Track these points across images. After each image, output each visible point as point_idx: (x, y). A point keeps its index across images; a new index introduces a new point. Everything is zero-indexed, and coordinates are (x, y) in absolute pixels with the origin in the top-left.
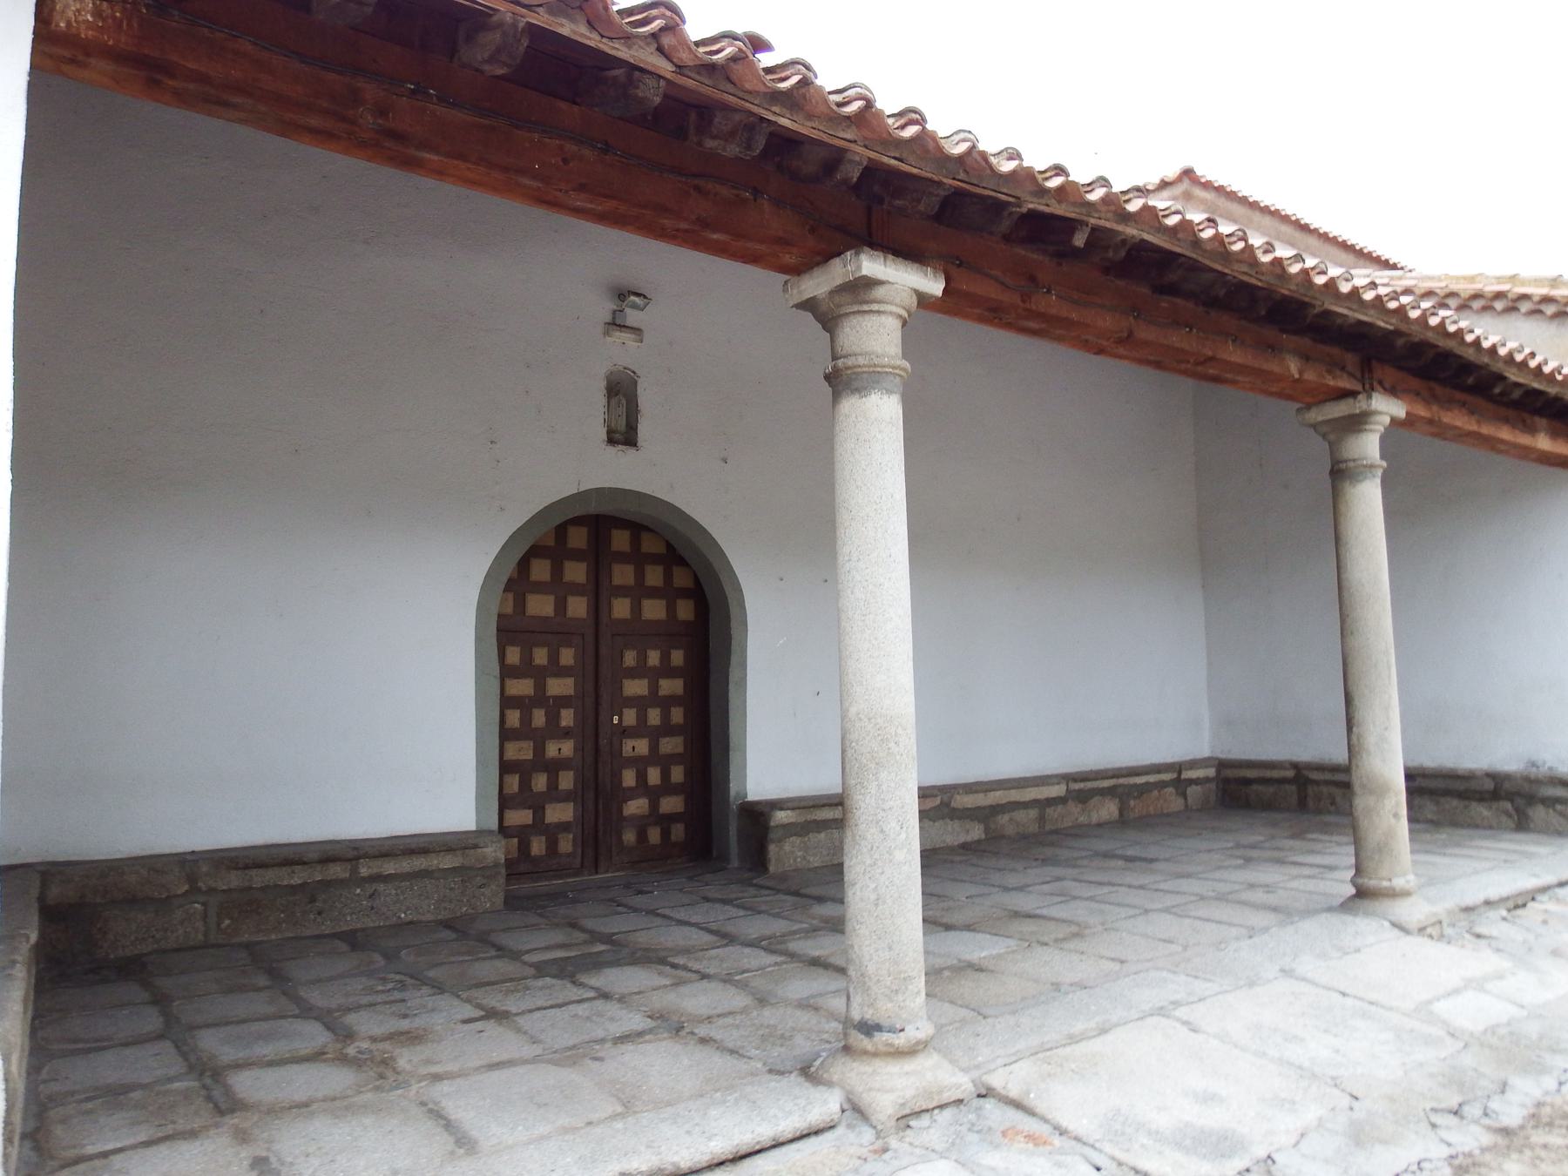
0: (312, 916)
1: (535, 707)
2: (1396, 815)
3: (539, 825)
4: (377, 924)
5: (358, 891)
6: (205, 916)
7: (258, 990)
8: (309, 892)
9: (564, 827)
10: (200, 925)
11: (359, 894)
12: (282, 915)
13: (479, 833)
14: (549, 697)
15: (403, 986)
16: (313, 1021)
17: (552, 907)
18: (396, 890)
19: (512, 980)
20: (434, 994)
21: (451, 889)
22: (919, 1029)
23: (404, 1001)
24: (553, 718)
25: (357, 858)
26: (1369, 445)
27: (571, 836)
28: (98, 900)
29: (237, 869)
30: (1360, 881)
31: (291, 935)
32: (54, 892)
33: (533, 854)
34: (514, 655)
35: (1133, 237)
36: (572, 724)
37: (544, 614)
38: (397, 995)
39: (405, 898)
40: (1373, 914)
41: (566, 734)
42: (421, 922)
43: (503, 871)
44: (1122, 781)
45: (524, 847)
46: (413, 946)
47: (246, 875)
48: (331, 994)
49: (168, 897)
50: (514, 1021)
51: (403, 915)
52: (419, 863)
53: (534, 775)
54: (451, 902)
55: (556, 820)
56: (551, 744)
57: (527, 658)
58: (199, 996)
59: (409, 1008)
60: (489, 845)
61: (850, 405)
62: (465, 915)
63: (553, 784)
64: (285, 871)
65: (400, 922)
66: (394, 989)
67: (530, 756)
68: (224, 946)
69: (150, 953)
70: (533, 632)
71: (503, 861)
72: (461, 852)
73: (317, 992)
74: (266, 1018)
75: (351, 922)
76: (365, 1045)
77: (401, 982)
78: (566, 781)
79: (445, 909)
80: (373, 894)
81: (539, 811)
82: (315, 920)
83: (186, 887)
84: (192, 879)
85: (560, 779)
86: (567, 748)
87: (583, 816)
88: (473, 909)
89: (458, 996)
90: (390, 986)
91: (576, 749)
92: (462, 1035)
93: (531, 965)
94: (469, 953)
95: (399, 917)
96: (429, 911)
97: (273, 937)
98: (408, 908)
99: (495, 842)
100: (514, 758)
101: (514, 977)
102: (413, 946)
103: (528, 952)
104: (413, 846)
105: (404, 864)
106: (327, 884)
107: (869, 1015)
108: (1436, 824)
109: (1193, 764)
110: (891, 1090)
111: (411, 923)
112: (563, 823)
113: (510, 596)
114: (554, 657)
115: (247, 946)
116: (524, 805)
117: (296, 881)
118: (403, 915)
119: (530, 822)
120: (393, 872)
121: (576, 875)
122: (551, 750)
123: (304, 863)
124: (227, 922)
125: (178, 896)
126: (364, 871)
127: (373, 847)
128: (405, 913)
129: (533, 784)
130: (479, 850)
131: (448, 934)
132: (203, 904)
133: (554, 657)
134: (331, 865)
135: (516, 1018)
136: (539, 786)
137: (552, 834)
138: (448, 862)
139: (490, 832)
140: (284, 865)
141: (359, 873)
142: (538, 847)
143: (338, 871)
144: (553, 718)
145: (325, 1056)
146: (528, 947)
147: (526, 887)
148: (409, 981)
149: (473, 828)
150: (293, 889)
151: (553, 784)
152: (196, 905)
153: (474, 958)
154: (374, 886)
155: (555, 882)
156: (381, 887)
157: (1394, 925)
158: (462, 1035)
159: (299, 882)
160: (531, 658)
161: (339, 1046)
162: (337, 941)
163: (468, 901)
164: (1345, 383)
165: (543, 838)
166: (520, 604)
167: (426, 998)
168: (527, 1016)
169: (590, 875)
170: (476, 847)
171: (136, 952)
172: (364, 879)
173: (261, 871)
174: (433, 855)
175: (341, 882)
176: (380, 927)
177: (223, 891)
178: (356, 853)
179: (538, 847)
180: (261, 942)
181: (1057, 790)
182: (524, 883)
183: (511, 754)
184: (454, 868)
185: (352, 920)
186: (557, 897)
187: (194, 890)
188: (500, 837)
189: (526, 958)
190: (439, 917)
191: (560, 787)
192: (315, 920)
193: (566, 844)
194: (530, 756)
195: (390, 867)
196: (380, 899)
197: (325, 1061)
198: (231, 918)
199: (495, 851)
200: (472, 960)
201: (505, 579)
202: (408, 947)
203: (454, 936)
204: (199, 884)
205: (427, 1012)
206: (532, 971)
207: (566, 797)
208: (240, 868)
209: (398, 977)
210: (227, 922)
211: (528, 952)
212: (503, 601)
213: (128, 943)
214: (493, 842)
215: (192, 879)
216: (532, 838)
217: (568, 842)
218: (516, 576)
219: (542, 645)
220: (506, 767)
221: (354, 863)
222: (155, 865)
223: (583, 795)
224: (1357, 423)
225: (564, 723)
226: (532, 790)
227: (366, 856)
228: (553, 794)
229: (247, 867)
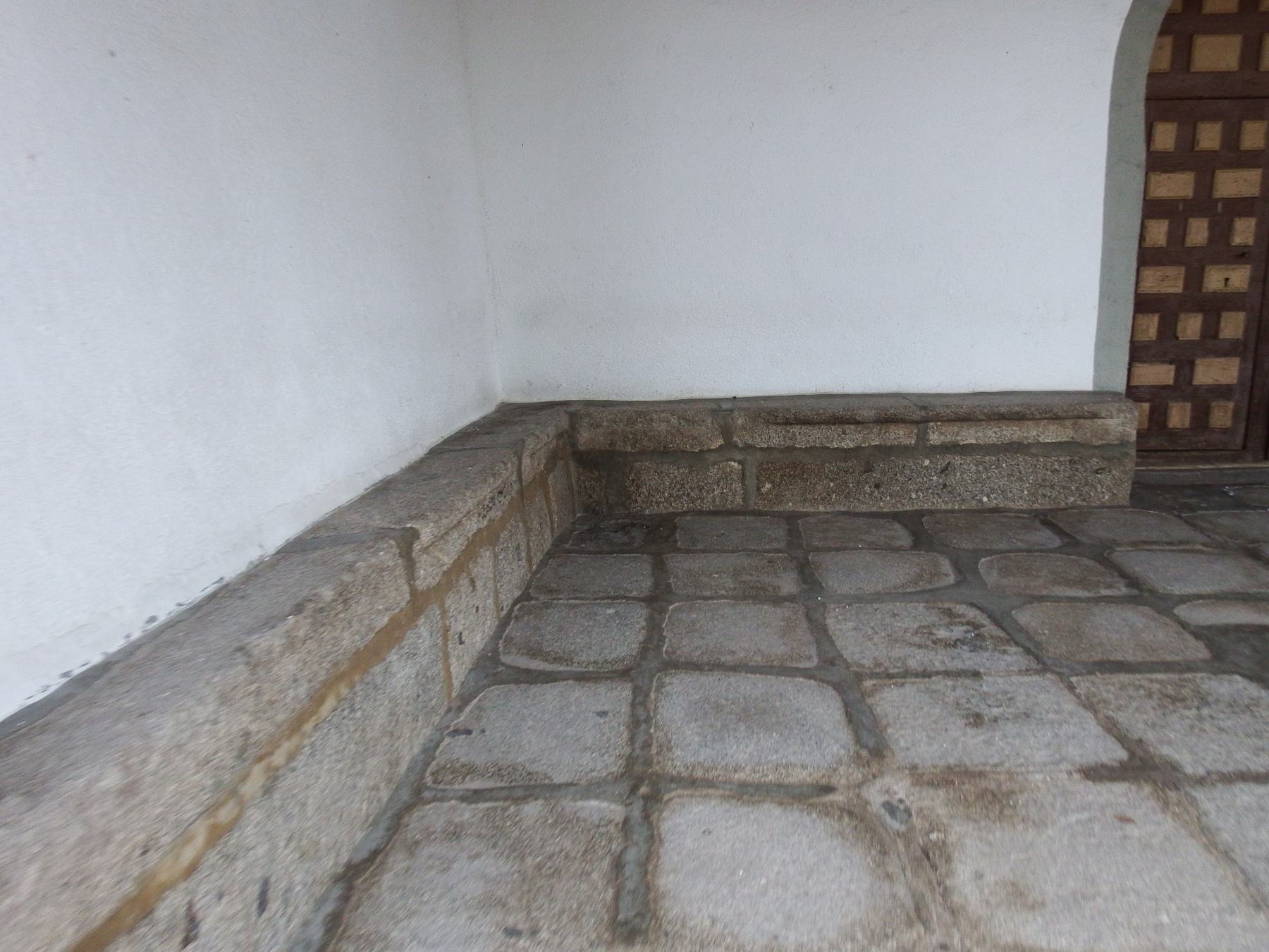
0: (867, 488)
1: (1192, 216)
3: (1183, 387)
4: (949, 507)
5: (927, 462)
6: (743, 477)
7: (777, 600)
8: (865, 459)
9: (1222, 392)
10: (737, 486)
11: (926, 467)
12: (832, 484)
13: (1098, 395)
14: (1217, 200)
15: (976, 642)
16: (831, 692)
17: (1203, 509)
18: (977, 466)
19: (1167, 667)
20: (1027, 671)
21: (1054, 471)
23: (976, 675)
24: (1221, 232)
25: (926, 421)
27: (1231, 405)
28: (629, 449)
29: (777, 424)
31: (843, 509)
32: (585, 437)
33: (1171, 426)
34: (1166, 137)
36: (1250, 241)
37: (1222, 66)
38: (968, 659)
39: (989, 478)
41: (1241, 256)
42: (1010, 510)
43: (1133, 452)
45: (1157, 419)
46: (997, 552)
47: (788, 432)
48: (870, 632)
49: (701, 451)
50: (1194, 802)
51: (985, 499)
52: (1011, 432)
53: (1182, 316)
54: (1052, 487)
55: (1210, 381)
56: (1212, 272)
57: (1188, 141)
58: (705, 598)
59: (984, 697)
60: (1115, 414)
62: (1073, 508)
63: (1210, 332)
64: (834, 430)
65: (979, 507)
66: (963, 642)
67: (1179, 289)
68: (766, 514)
69: (685, 513)
70: (1200, 98)
71: (1133, 438)
72: (1072, 421)
73: (851, 624)
74: (767, 669)
75: (916, 501)
76: (901, 788)
77: (976, 626)
78: (1233, 326)
79: (1044, 496)
80: (946, 468)
81: (1185, 365)
82: (871, 494)
83: (720, 442)
84: (727, 432)
85: (1223, 324)
86: (1240, 278)
87: (1253, 379)
88: (1084, 500)
89: (1071, 688)
90: (958, 632)
91: (1253, 280)
92: (1086, 815)
93: (1200, 633)
94: (1082, 582)
95: (980, 501)
96: (1021, 497)
97: (821, 508)
98: (993, 490)
99: (1124, 412)
100: (1155, 291)
101: (1169, 658)
102: (997, 552)
103: (1184, 599)
104: (1003, 410)
105: (990, 433)
106: (886, 451)
111: (995, 510)
112: (1220, 386)
113: (1168, 41)
114: (1232, 138)
115: (791, 519)
116: (1161, 358)
117: (848, 443)
118: (985, 499)
119: (1171, 382)
120: (974, 442)
121: (1234, 460)
122: (1214, 280)
123: (858, 423)
124: (768, 486)
125: (710, 451)
126: (935, 438)
127: (947, 407)
128: (988, 496)
129: (1179, 329)
130: (1099, 422)
131: (1044, 537)
132: (740, 462)
133: (1232, 138)
134: (892, 428)
135: (1199, 794)
136: (1189, 332)
137: (1202, 400)
138: (1052, 434)
139: (1115, 395)
140: (834, 424)
141: (928, 440)
142: (1179, 416)
143: (900, 435)
144: (1221, 232)
145: (829, 798)
146: (1191, 590)
147: (1160, 470)
148: (990, 628)
149: (1088, 386)
150: (846, 454)
151: (1210, 332)
152: (733, 463)
153: (1092, 595)
154: (948, 458)
155: (1201, 467)
156: (958, 460)
158: (1086, 815)
159: (851, 446)
160: (1194, 141)
161: (857, 775)
162: (897, 526)
163: (1077, 489)
165: (1188, 406)
166: (1184, 52)
167: (1014, 679)
168: (1221, 793)
169: (1258, 462)
170: (1095, 416)
171: (671, 510)
172: (934, 447)
173: (805, 429)
174: (1030, 423)
175: (904, 450)
176: (953, 511)
177: (762, 449)
178: (923, 413)
179: (1179, 416)
180: (806, 515)
182: (1153, 465)
183: (1148, 285)
184: (1060, 443)
185: (918, 497)
186: (1207, 491)
187: (729, 445)
188: (1130, 404)
189: (1182, 611)
190: (1036, 506)
191: (1222, 336)
192: (871, 494)
193: (1222, 416)
194: (1179, 289)
195: (969, 436)
196: (955, 475)
197: (826, 811)
198: (772, 482)
199: (1123, 424)
200: (1087, 600)
201: (1159, 17)
202: (989, 552)
203: (1057, 542)
204: (735, 439)
205: (1016, 717)
206: (1199, 651)
207: (1232, 349)
208: (779, 424)
209: (972, 614)
210: (768, 486)
211: (1184, 599)
212: (1159, 48)
213: (663, 500)
214: (1120, 411)
215: (727, 432)
216: (1171, 404)
217: (1226, 412)
218: (1179, 8)
219: (1214, 118)
220: (1143, 304)
221: (921, 426)
222: (685, 410)
223: (1256, 349)
225: (1237, 240)
226: (1177, 338)
227: (938, 418)
228: (1210, 343)
229: (787, 423)
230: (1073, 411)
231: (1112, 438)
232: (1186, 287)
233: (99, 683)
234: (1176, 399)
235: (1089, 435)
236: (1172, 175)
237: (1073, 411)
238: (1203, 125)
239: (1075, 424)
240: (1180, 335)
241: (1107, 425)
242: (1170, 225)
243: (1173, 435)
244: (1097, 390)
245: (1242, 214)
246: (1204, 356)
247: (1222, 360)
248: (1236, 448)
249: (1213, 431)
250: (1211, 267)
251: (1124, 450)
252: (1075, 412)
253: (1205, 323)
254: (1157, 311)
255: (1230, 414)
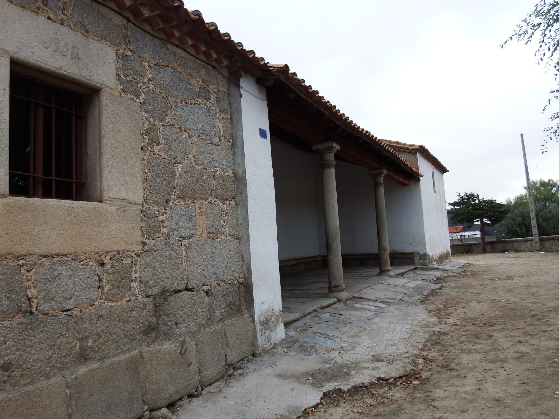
2: (388, 255)
22: (344, 287)
26: (382, 179)
30: (381, 269)
35: (96, 185)
40: (385, 275)
44: (305, 260)
61: (327, 170)
107: (336, 284)
108: (346, 273)
109: (318, 256)
110: (344, 296)
157: (389, 276)
164: (379, 166)
181: (293, 262)
224: (380, 175)
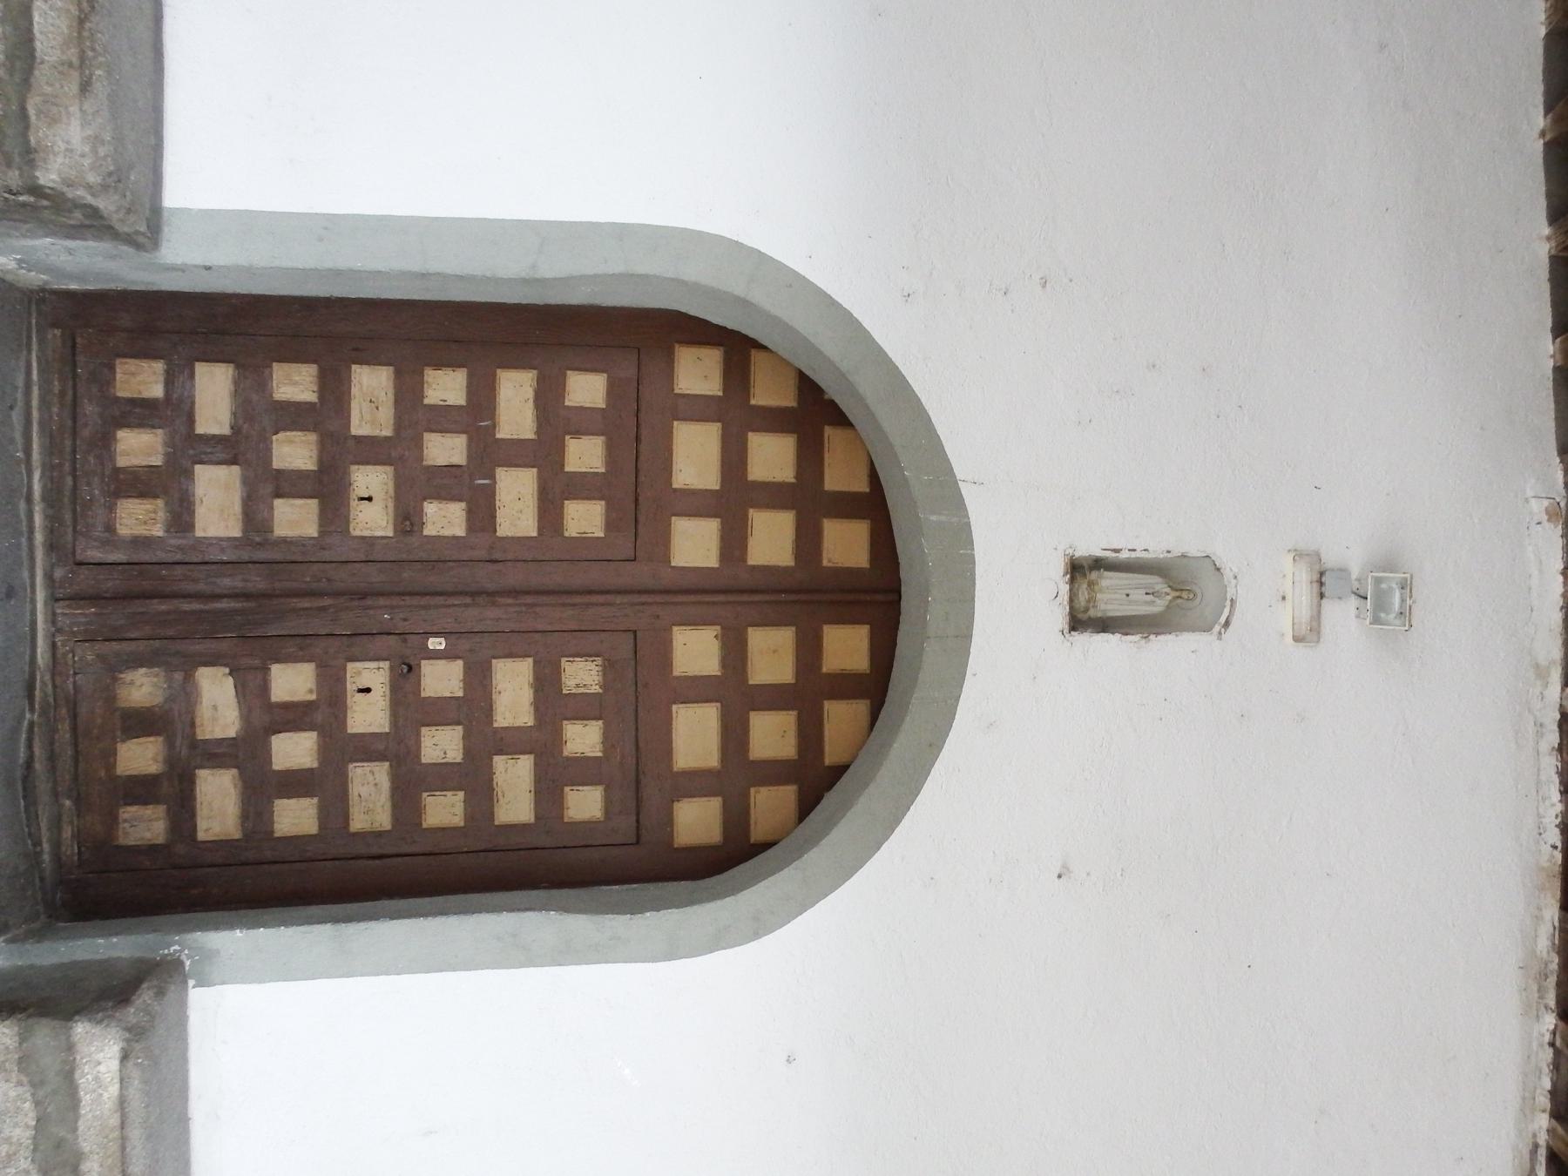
9: (182, 516)
14: (493, 477)
24: (445, 483)
27: (158, 531)
41: (408, 519)
53: (312, 437)
63: (288, 484)
81: (228, 449)
99: (94, 151)
100: (355, 391)
112: (192, 513)
114: (582, 486)
119: (201, 429)
122: (370, 480)
133: (582, 486)
136: (286, 449)
144: (445, 483)
149: (172, 198)
151: (288, 484)
165: (157, 460)
207: (255, 518)
225: (431, 509)
230: (93, 50)
231: (40, 133)
232: (359, 440)
233: (83, 567)
234: (169, 443)
235: (48, 89)
236: (531, 404)
237: (93, 50)
238: (600, 442)
239: (71, 65)
240: (281, 435)
241: (69, 124)
242: (460, 407)
243: (105, 442)
244: (165, 214)
245: (470, 513)
246: (246, 481)
247: (237, 508)
248: (79, 551)
249: (111, 508)
250: (391, 475)
251: (17, 159)
252: (90, 54)
253: (300, 474)
254: (321, 397)
255: (141, 531)
